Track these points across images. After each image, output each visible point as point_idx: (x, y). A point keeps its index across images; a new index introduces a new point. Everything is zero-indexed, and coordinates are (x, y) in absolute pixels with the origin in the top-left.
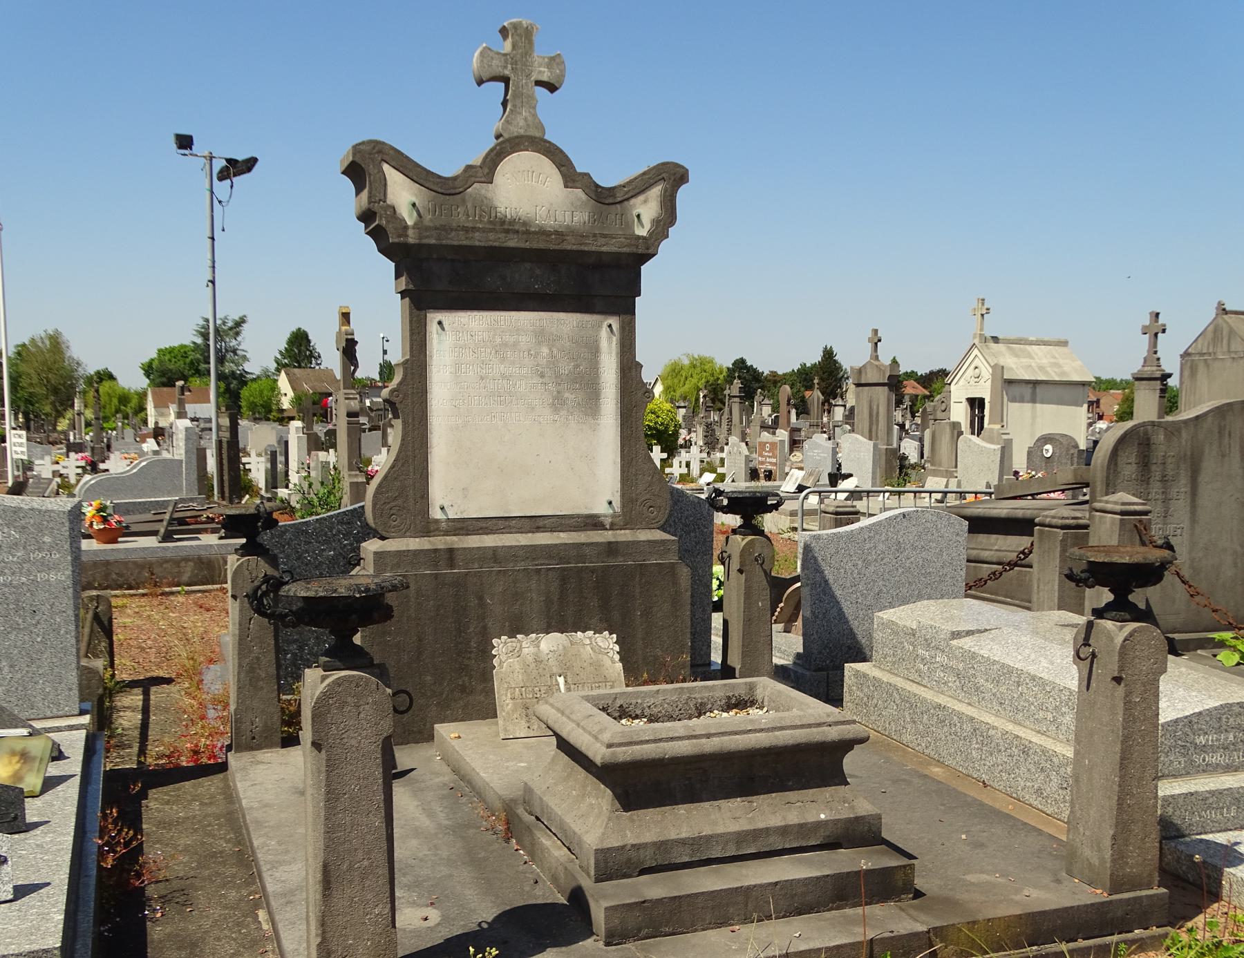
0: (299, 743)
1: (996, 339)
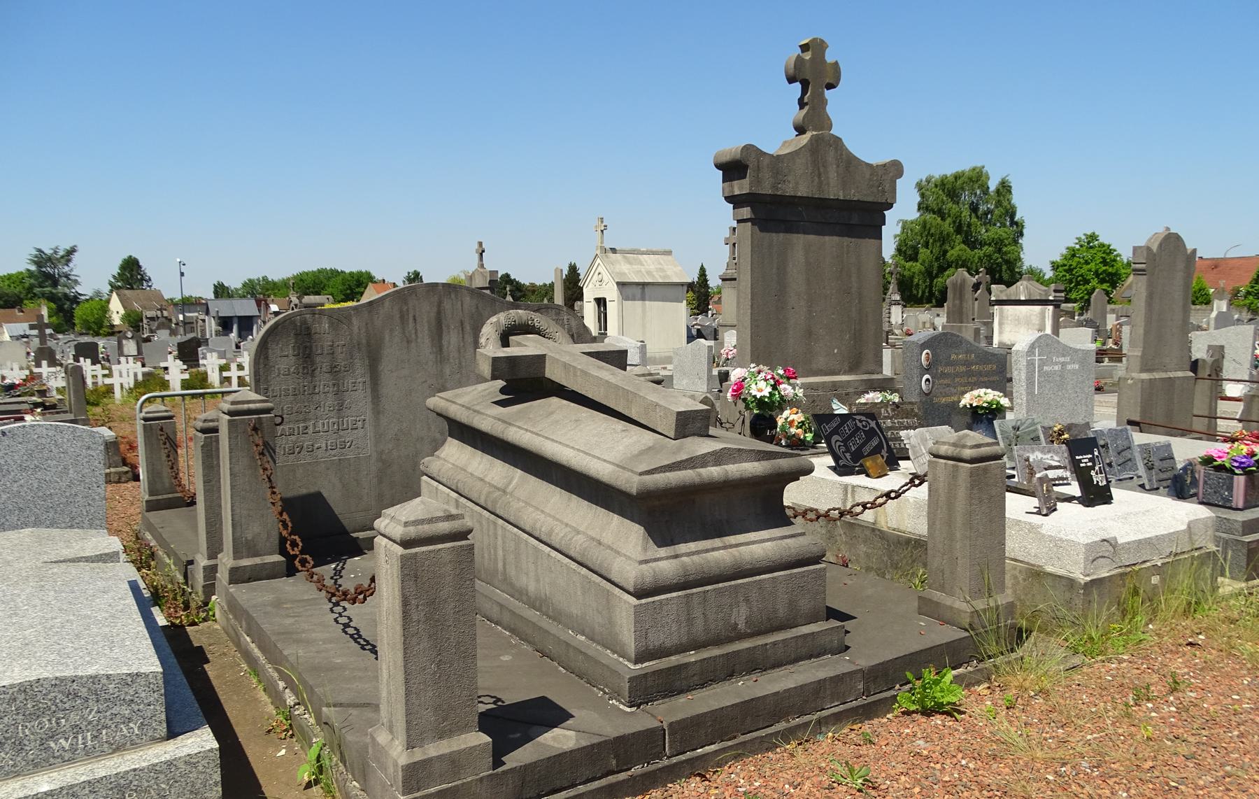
0: (1222, 347)
1: (614, 250)
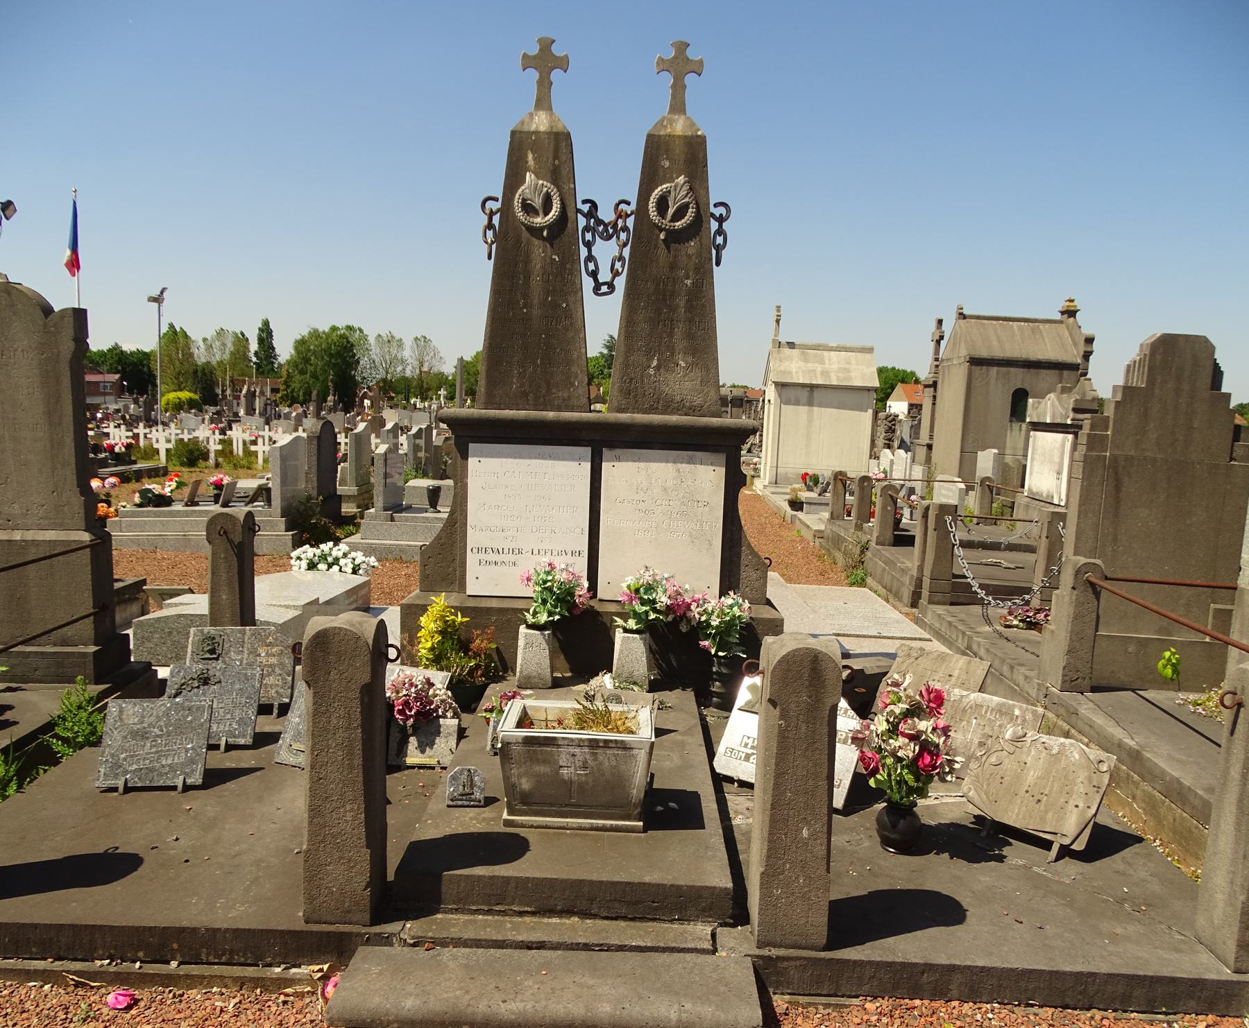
1: (791, 345)
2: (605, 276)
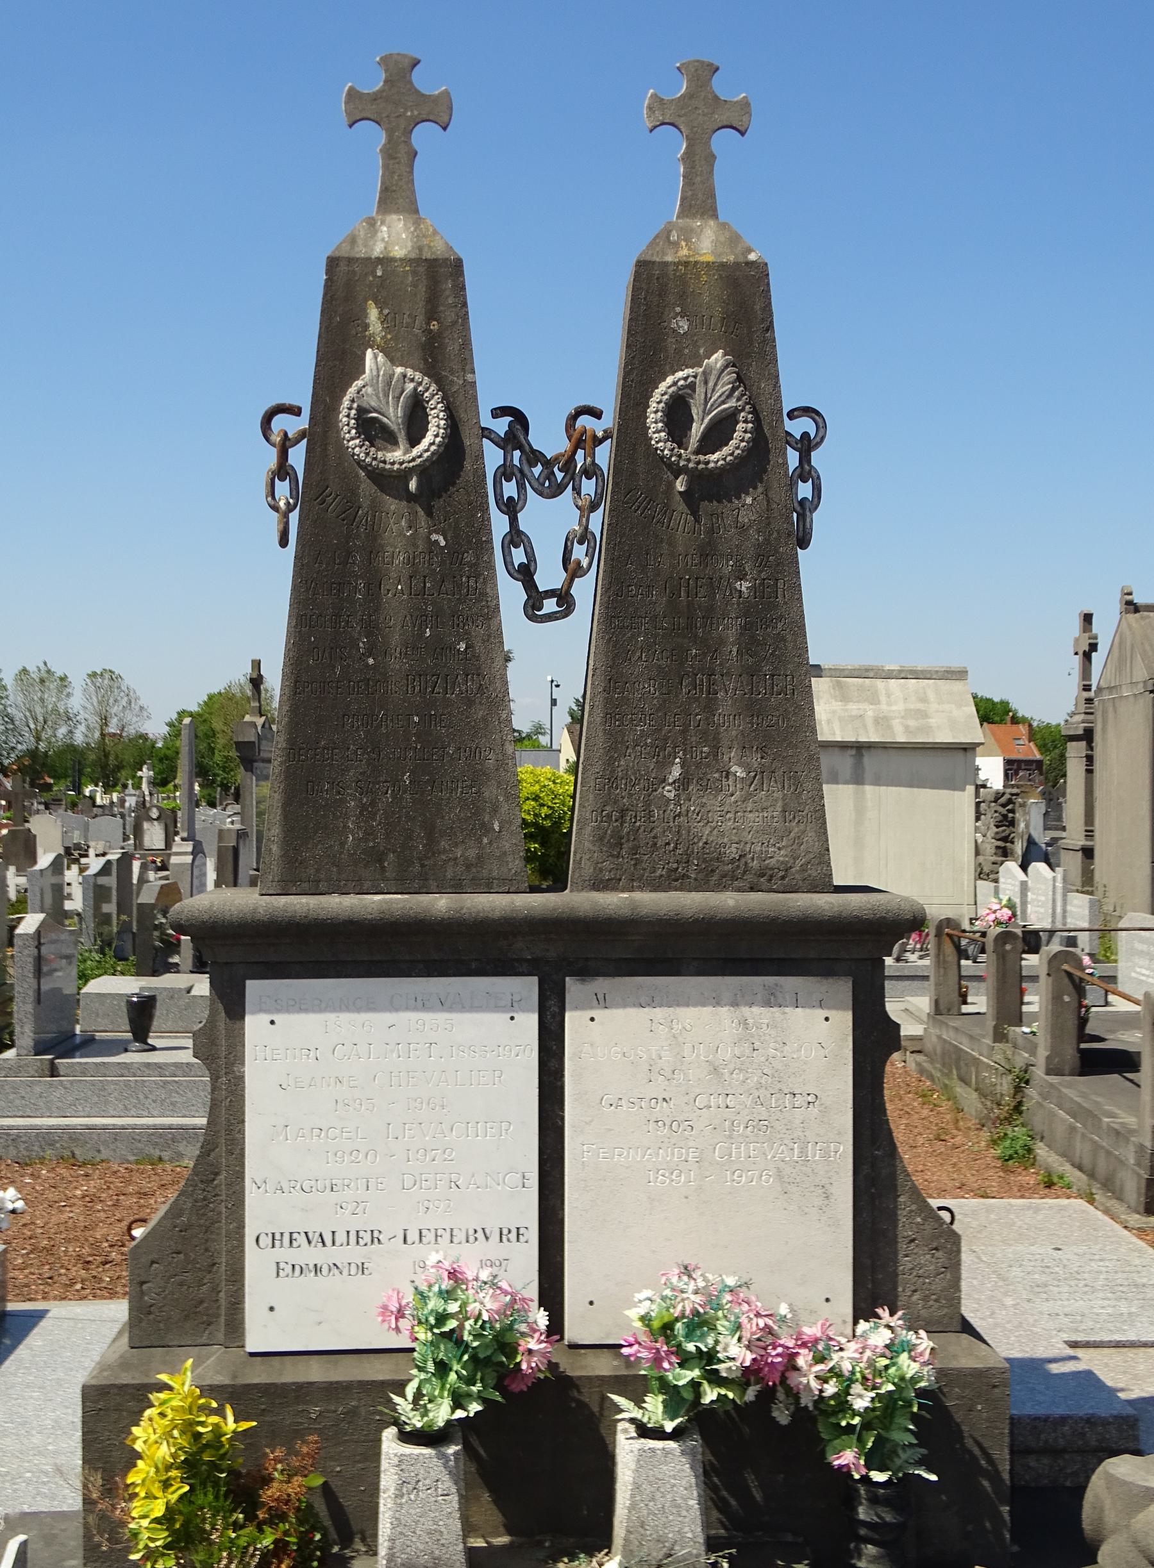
2: (549, 576)
